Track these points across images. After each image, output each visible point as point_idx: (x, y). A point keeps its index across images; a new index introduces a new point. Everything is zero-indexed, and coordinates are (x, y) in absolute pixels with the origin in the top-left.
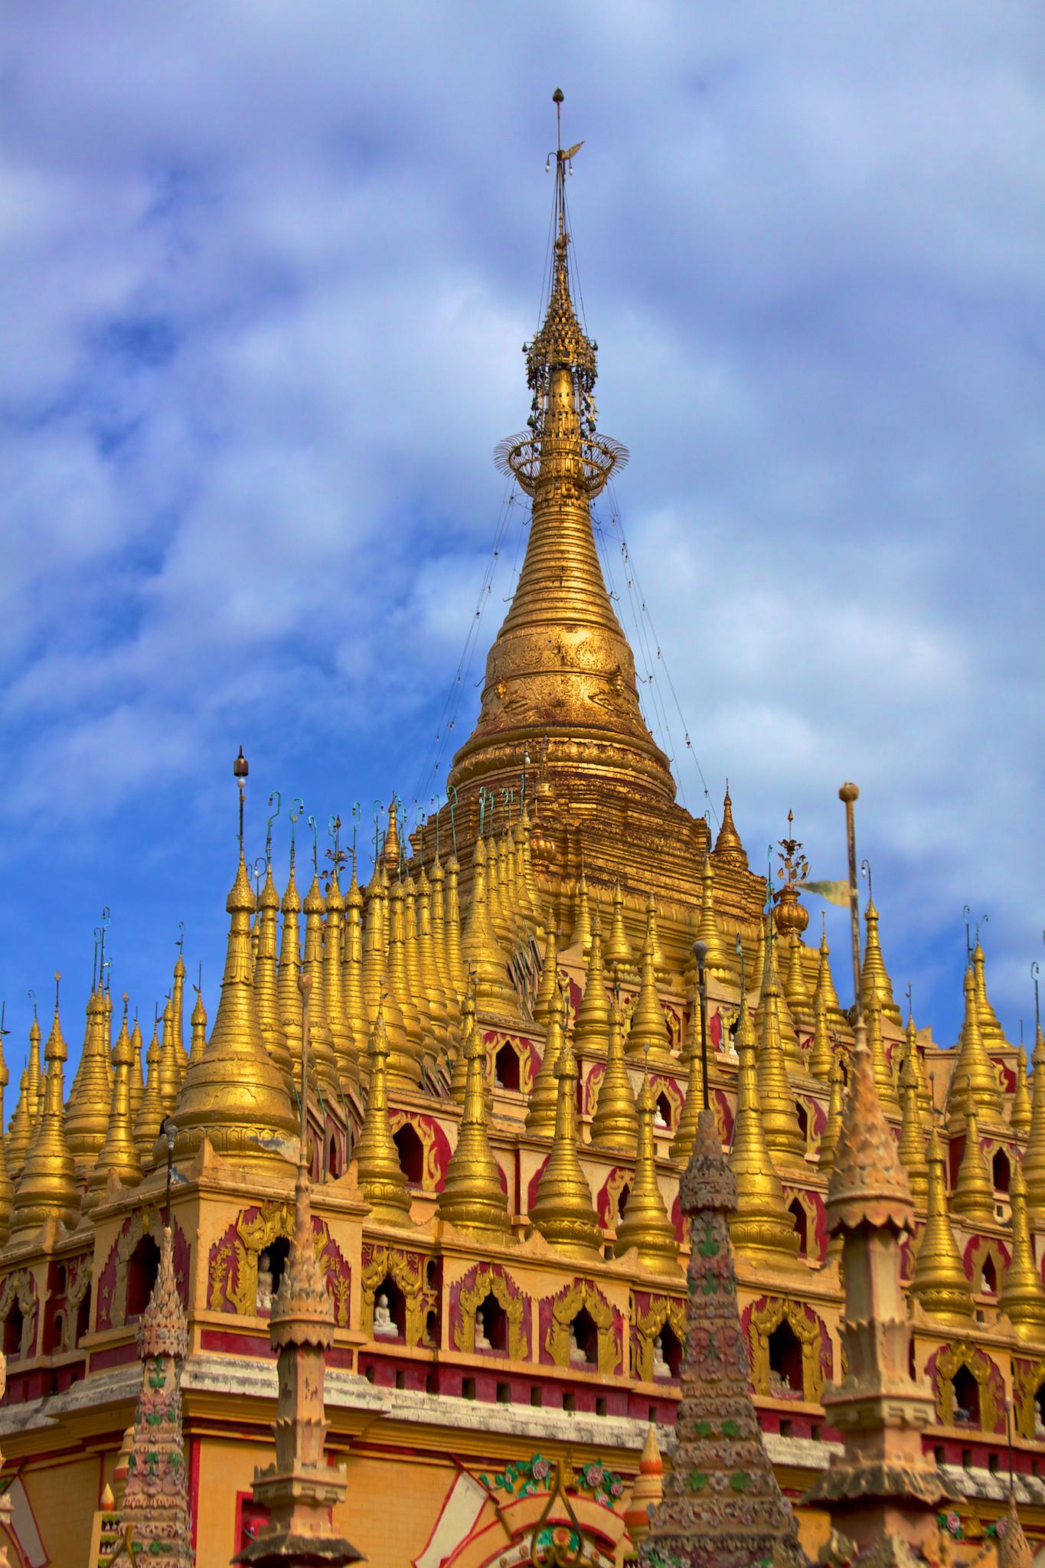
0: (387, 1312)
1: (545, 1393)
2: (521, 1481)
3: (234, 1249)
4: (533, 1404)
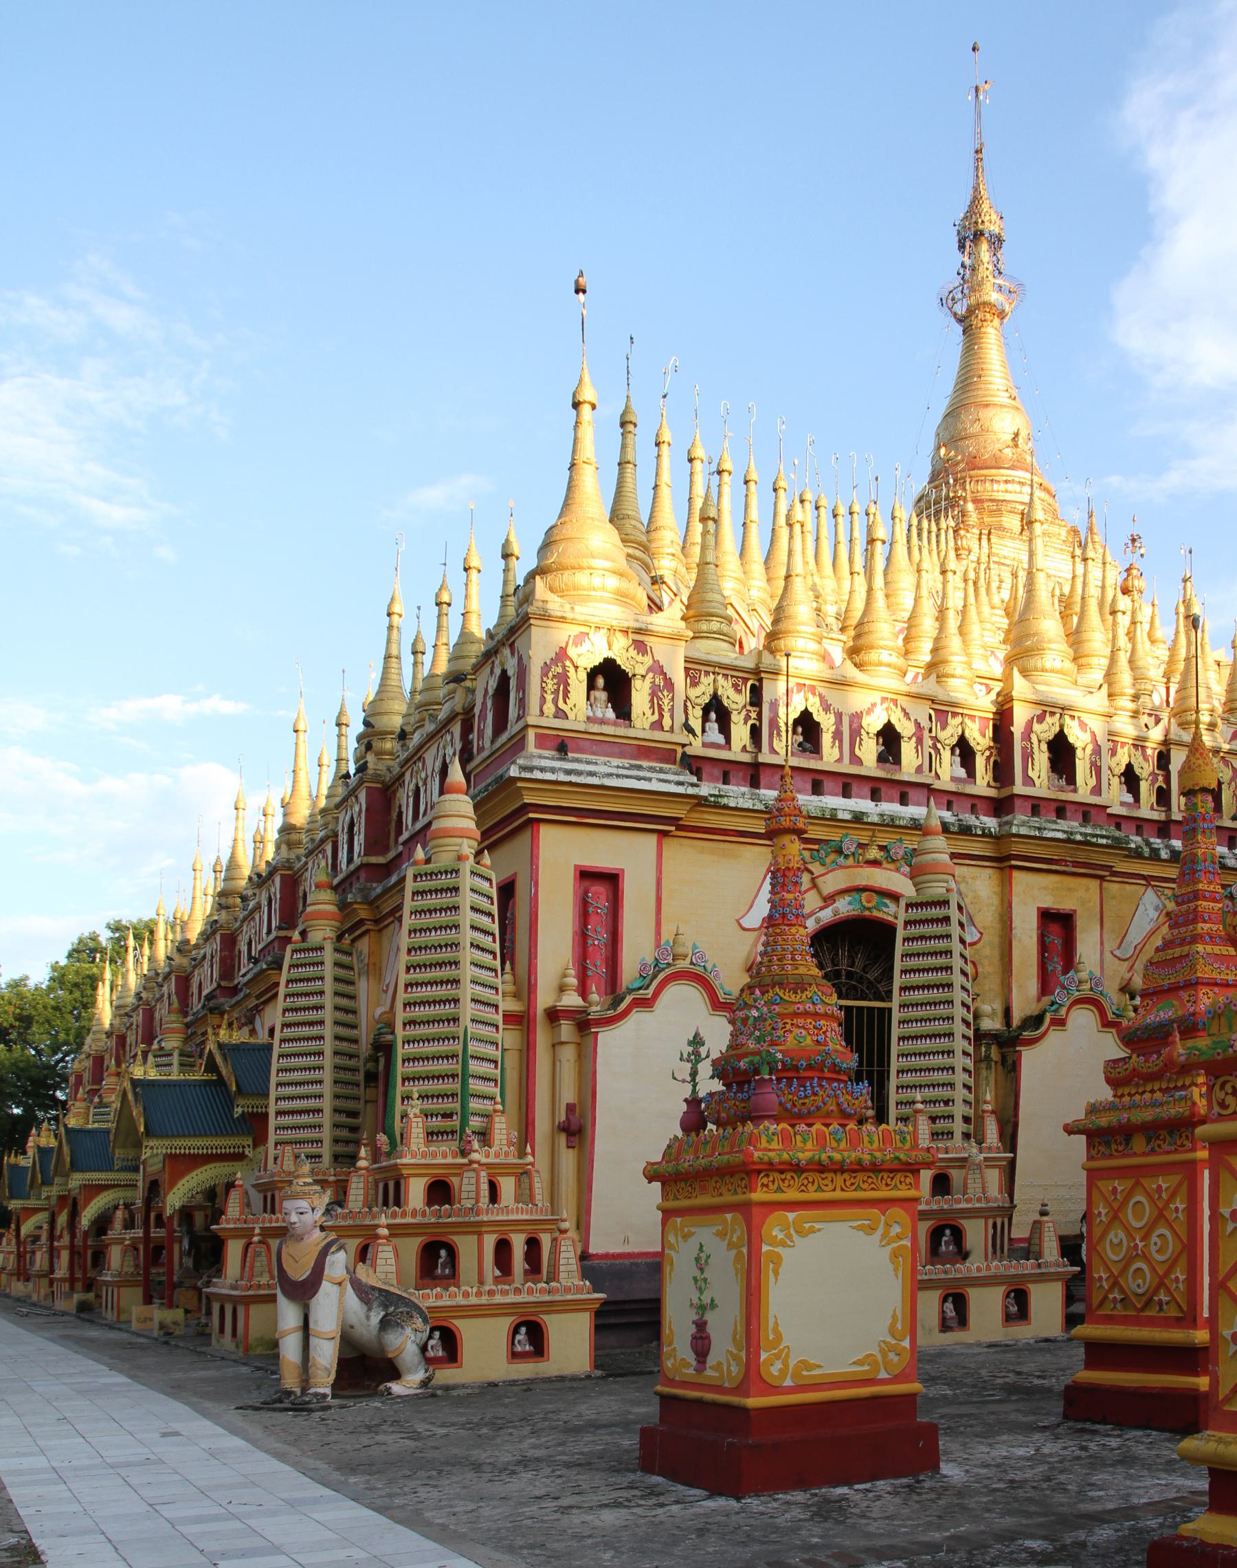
0: (716, 726)
1: (855, 788)
2: (833, 856)
3: (564, 667)
4: (844, 796)
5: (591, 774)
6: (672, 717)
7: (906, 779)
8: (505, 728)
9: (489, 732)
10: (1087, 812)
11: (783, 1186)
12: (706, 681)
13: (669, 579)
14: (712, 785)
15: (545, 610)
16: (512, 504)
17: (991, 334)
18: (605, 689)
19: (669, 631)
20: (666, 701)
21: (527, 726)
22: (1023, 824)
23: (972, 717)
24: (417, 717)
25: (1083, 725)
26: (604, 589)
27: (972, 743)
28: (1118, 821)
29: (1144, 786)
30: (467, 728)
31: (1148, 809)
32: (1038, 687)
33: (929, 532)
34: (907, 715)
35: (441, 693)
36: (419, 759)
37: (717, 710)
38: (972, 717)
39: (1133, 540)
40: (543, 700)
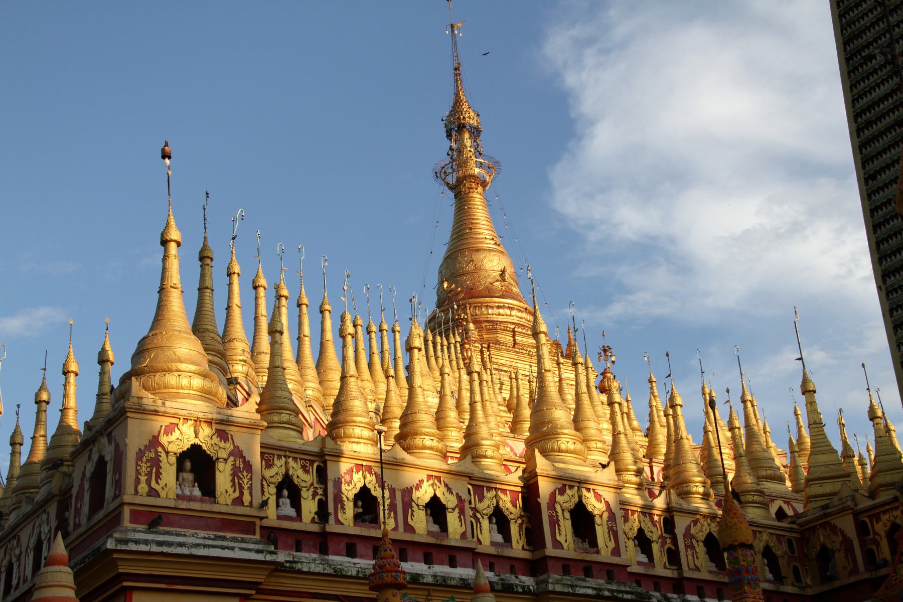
0: (288, 501)
1: (410, 553)
3: (156, 452)
5: (181, 545)
6: (251, 494)
7: (453, 544)
8: (102, 506)
9: (86, 510)
10: (611, 571)
12: (279, 463)
13: (242, 380)
14: (287, 552)
15: (141, 405)
16: (107, 320)
17: (477, 199)
18: (191, 471)
19: (247, 421)
20: (246, 481)
21: (123, 504)
22: (557, 582)
23: (504, 491)
24: (15, 499)
25: (598, 497)
26: (190, 388)
27: (506, 513)
28: (638, 578)
29: (655, 547)
30: (63, 507)
31: (661, 569)
32: (556, 464)
33: (442, 346)
34: (449, 490)
35: (38, 478)
36: (14, 537)
37: (289, 488)
38: (504, 491)
39: (605, 351)
40: (138, 482)
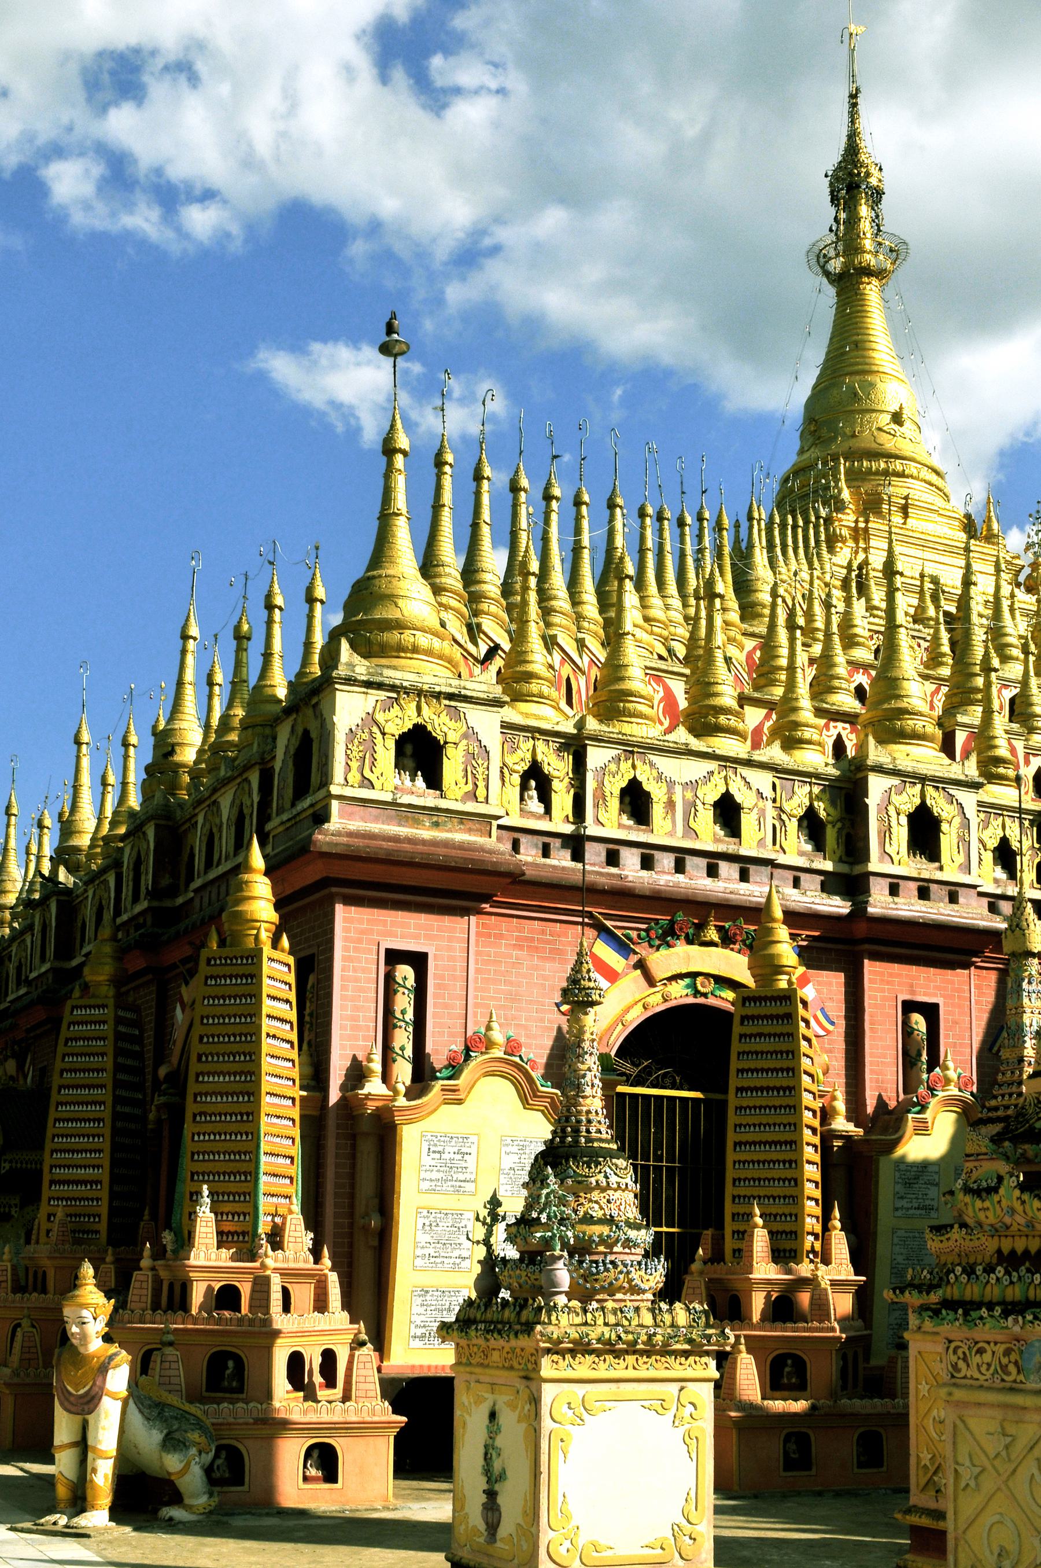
3: (371, 733)
11: (575, 1364)
17: (872, 290)
20: (480, 770)
37: (536, 778)
